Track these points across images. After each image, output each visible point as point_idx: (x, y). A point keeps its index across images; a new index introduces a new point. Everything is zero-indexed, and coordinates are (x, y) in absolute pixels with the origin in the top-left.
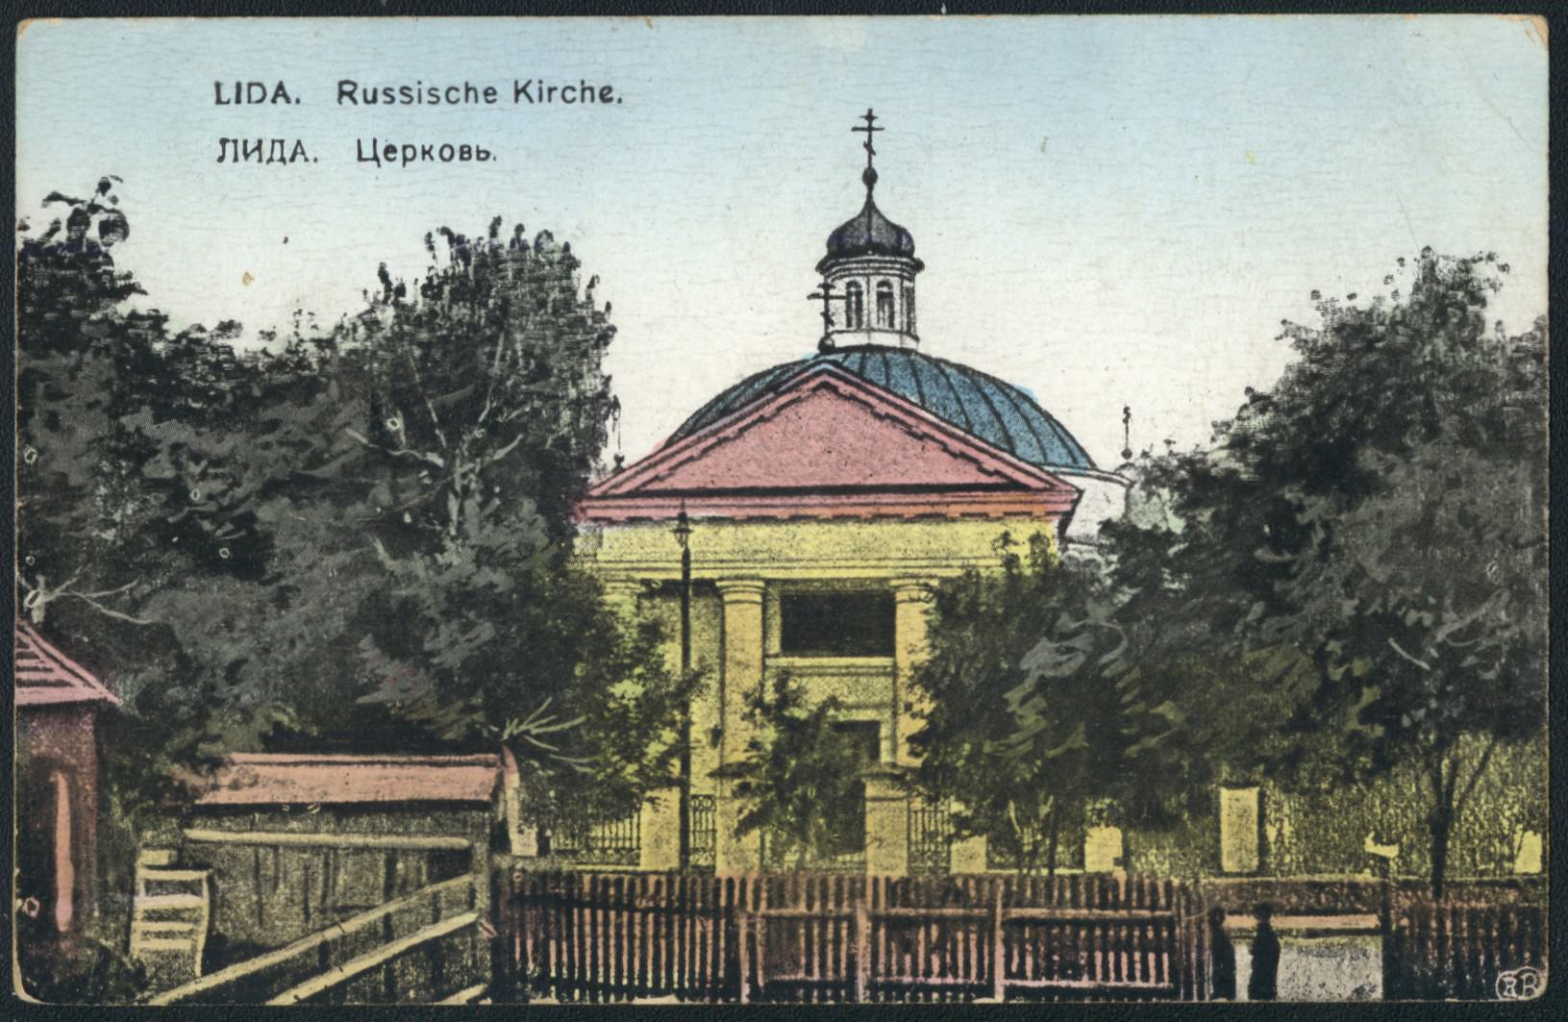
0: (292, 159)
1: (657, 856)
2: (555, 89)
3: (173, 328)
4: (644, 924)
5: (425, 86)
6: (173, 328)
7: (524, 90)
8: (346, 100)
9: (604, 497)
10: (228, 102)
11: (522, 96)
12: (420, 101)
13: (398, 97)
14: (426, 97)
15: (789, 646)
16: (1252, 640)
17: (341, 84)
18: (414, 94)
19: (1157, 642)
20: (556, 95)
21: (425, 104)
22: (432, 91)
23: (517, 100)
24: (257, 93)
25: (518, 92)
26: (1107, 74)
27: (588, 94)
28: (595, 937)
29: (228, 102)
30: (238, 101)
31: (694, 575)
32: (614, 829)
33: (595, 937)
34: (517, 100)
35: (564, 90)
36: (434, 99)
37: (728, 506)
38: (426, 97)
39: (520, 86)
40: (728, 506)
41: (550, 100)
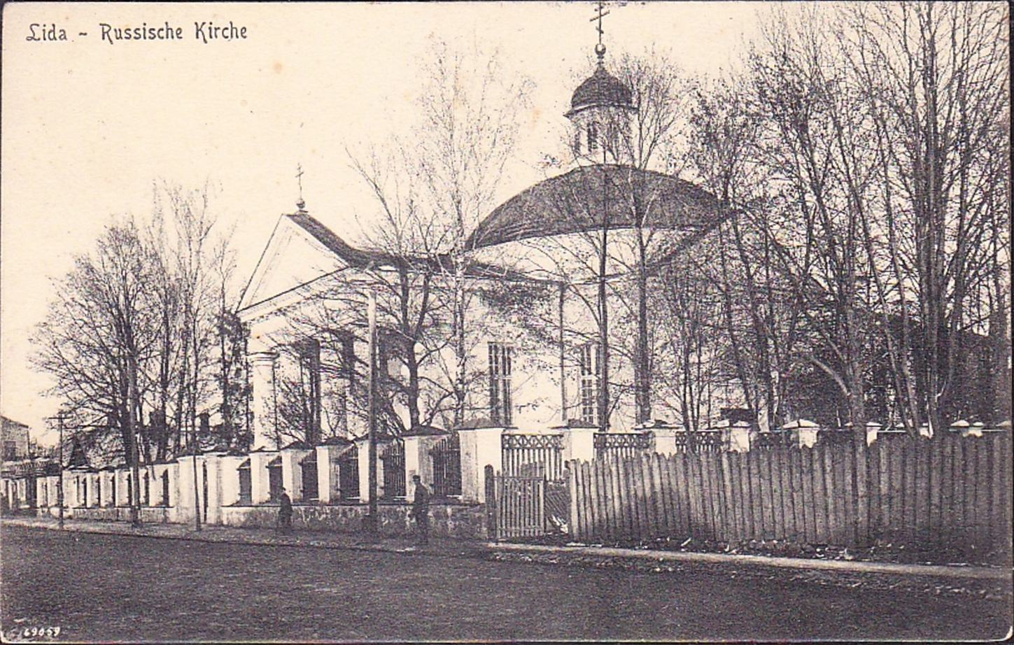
2: (219, 28)
3: (683, 76)
6: (683, 76)
10: (39, 39)
12: (145, 38)
13: (124, 35)
14: (148, 34)
20: (220, 32)
24: (227, 33)
26: (608, 627)
28: (534, 510)
29: (39, 39)
30: (167, 37)
31: (192, 457)
32: (786, 327)
33: (534, 510)
35: (159, 30)
36: (128, 36)
38: (148, 34)
41: (216, 37)
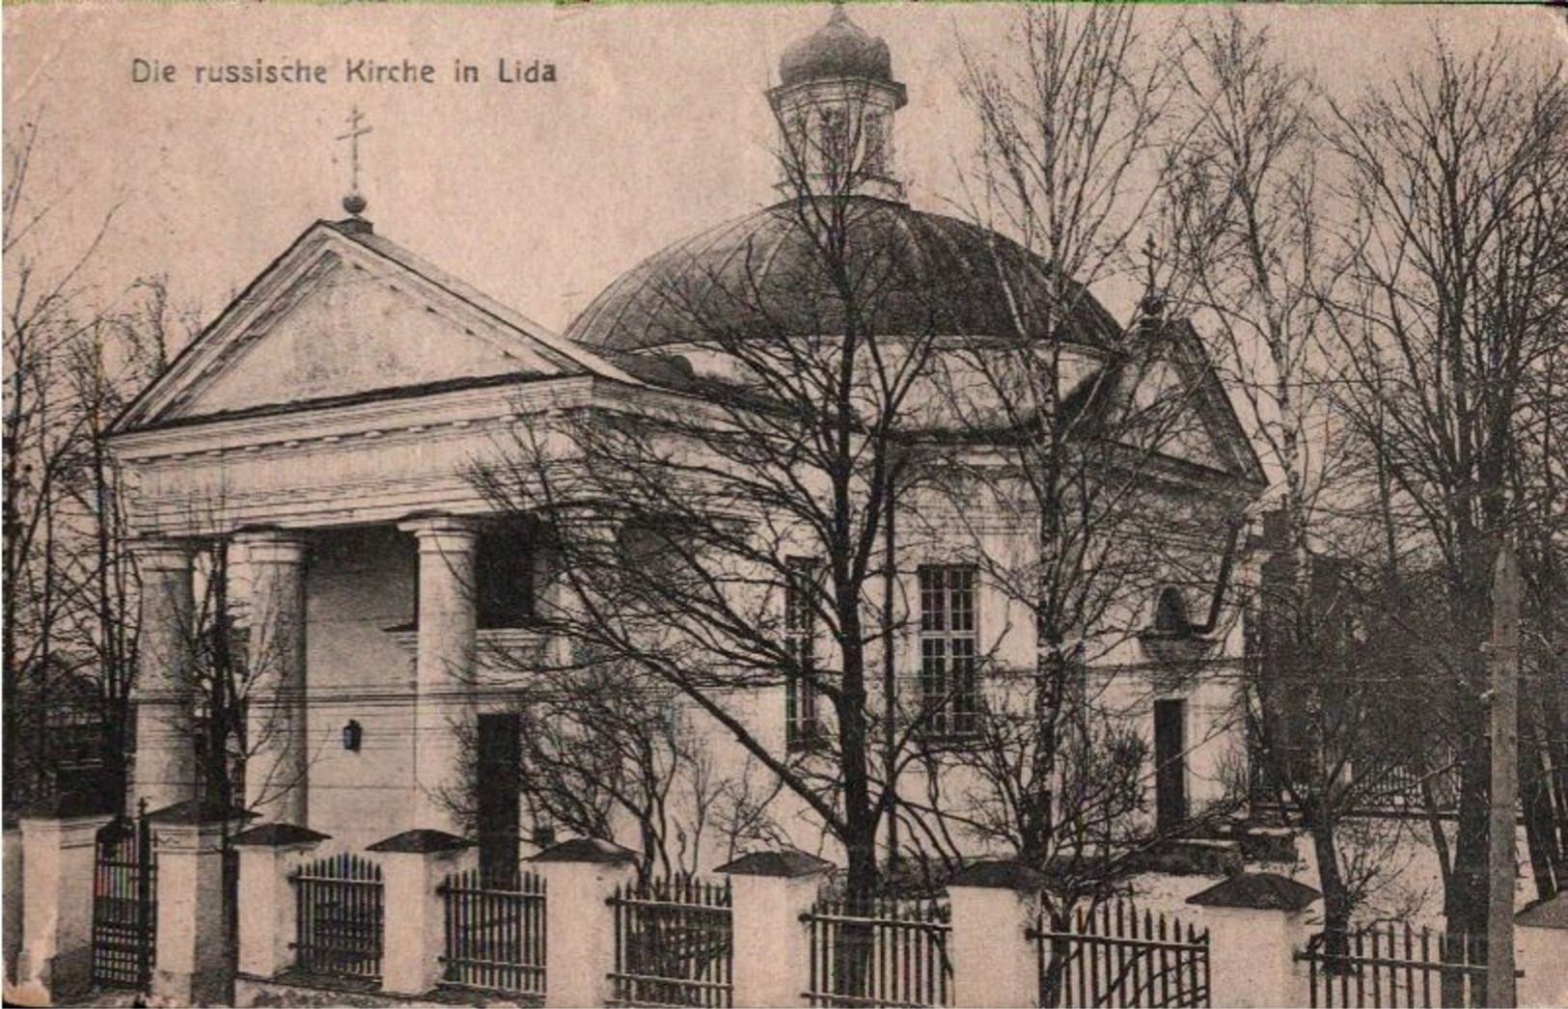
0: (1299, 76)
1: (879, 790)
4: (918, 940)
5: (264, 66)
7: (357, 70)
8: (354, 76)
9: (1056, 244)
11: (354, 76)
14: (265, 74)
15: (480, 625)
16: (1252, 609)
17: (475, 69)
18: (254, 73)
19: (658, 870)
20: (385, 74)
21: (264, 82)
22: (271, 69)
23: (349, 79)
25: (350, 72)
27: (303, 73)
34: (349, 79)
37: (336, 420)
38: (265, 74)
39: (354, 66)
40: (336, 420)
